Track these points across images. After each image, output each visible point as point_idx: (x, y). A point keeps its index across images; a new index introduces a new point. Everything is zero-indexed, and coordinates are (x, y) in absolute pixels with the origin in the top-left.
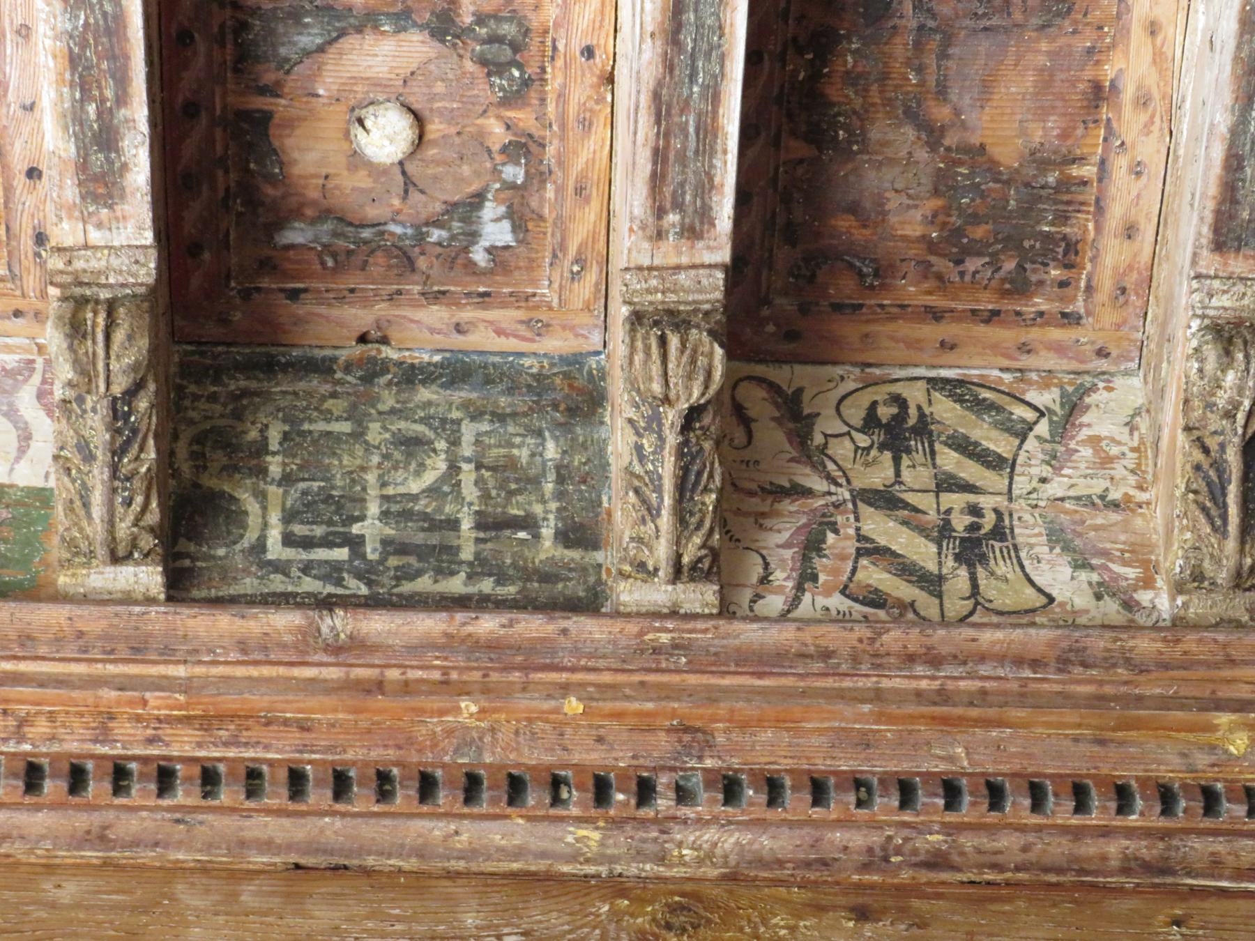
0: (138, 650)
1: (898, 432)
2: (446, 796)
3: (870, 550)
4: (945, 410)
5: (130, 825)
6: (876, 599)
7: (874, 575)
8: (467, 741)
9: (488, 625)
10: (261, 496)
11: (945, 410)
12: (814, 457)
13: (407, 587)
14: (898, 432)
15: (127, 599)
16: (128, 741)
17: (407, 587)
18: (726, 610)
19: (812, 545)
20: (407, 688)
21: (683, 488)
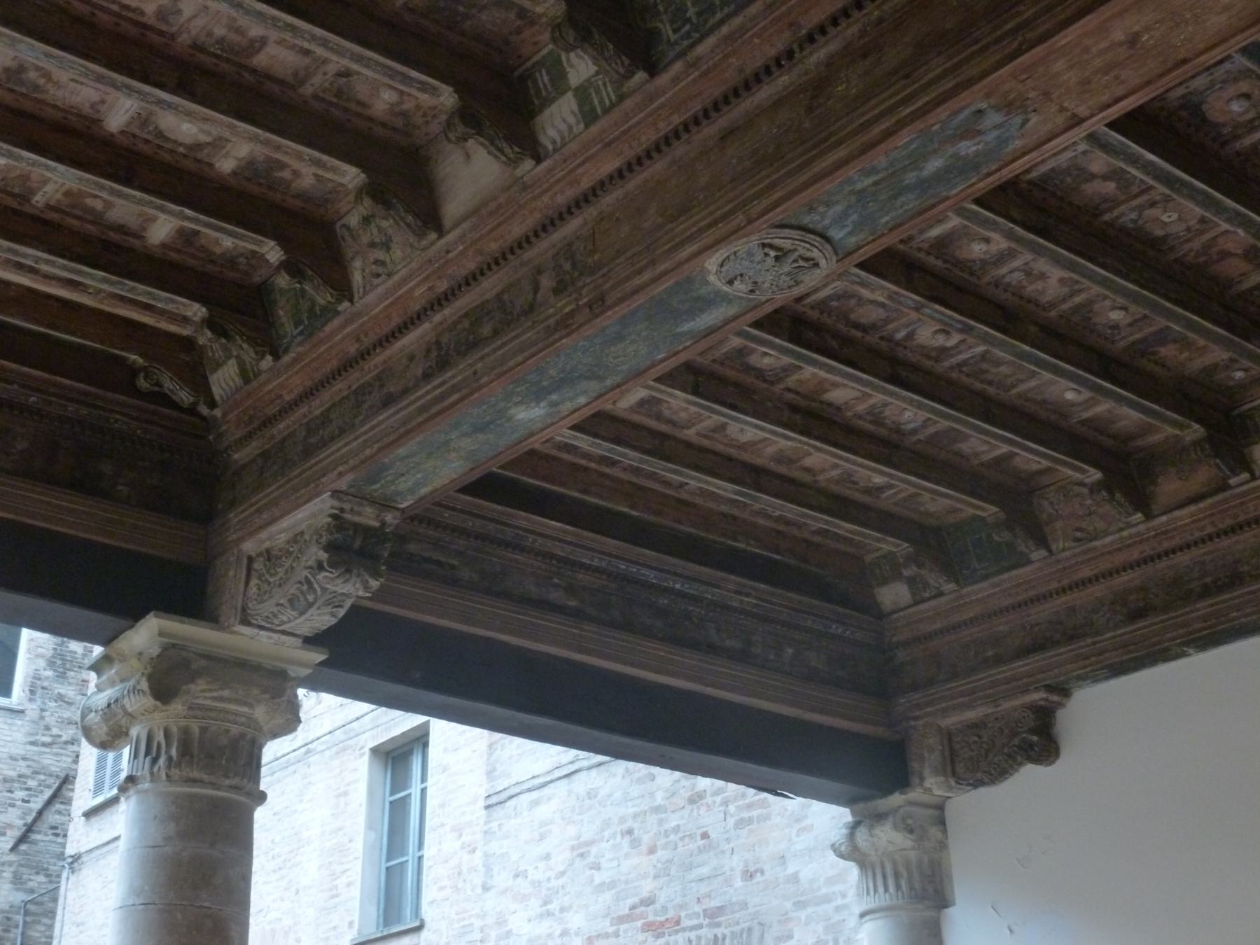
0: (652, 99)
8: (741, 70)
10: (661, 21)
13: (708, 26)
17: (708, 26)
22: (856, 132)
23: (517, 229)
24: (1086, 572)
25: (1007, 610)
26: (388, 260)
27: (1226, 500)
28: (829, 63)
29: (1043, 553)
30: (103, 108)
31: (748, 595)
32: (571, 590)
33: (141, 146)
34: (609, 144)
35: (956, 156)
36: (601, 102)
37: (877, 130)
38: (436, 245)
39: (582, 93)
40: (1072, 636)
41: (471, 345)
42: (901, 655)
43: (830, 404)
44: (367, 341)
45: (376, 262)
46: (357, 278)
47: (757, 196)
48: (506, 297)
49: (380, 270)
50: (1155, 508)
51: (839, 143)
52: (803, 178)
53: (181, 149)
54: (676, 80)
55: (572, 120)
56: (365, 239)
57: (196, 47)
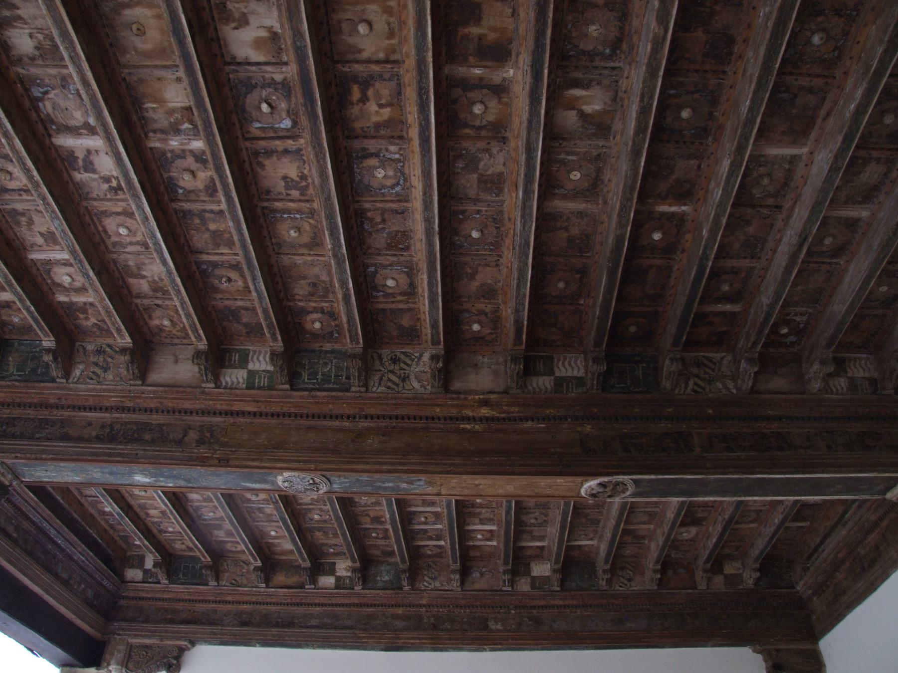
0: (286, 398)
1: (395, 360)
2: (484, 356)
3: (390, 380)
4: (402, 357)
5: (285, 422)
6: (389, 388)
7: (390, 384)
8: (331, 410)
9: (334, 394)
11: (402, 357)
12: (382, 365)
14: (395, 360)
15: (284, 390)
16: (285, 410)
18: (367, 391)
19: (381, 379)
20: (322, 403)
21: (359, 377)
22: (375, 463)
23: (188, 405)
24: (229, 598)
25: (186, 601)
26: (102, 375)
27: (301, 592)
28: (368, 429)
29: (216, 584)
30: (36, 248)
31: (83, 556)
32: (17, 528)
33: (34, 271)
34: (258, 401)
35: (398, 486)
36: (259, 382)
37: (385, 467)
38: (138, 387)
39: (252, 374)
40: (211, 623)
41: (131, 439)
42: (122, 602)
43: (186, 498)
44: (64, 402)
45: (94, 373)
46: (77, 373)
47: (324, 462)
48: (164, 428)
49: (94, 377)
50: (271, 585)
51: (368, 463)
52: (347, 467)
53: (49, 281)
54: (302, 397)
55: (241, 380)
56: (92, 359)
57: (115, 262)
